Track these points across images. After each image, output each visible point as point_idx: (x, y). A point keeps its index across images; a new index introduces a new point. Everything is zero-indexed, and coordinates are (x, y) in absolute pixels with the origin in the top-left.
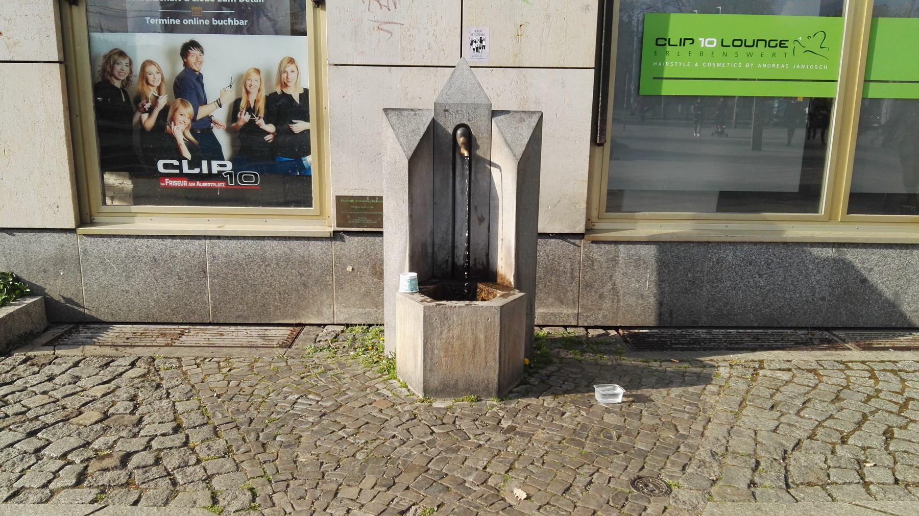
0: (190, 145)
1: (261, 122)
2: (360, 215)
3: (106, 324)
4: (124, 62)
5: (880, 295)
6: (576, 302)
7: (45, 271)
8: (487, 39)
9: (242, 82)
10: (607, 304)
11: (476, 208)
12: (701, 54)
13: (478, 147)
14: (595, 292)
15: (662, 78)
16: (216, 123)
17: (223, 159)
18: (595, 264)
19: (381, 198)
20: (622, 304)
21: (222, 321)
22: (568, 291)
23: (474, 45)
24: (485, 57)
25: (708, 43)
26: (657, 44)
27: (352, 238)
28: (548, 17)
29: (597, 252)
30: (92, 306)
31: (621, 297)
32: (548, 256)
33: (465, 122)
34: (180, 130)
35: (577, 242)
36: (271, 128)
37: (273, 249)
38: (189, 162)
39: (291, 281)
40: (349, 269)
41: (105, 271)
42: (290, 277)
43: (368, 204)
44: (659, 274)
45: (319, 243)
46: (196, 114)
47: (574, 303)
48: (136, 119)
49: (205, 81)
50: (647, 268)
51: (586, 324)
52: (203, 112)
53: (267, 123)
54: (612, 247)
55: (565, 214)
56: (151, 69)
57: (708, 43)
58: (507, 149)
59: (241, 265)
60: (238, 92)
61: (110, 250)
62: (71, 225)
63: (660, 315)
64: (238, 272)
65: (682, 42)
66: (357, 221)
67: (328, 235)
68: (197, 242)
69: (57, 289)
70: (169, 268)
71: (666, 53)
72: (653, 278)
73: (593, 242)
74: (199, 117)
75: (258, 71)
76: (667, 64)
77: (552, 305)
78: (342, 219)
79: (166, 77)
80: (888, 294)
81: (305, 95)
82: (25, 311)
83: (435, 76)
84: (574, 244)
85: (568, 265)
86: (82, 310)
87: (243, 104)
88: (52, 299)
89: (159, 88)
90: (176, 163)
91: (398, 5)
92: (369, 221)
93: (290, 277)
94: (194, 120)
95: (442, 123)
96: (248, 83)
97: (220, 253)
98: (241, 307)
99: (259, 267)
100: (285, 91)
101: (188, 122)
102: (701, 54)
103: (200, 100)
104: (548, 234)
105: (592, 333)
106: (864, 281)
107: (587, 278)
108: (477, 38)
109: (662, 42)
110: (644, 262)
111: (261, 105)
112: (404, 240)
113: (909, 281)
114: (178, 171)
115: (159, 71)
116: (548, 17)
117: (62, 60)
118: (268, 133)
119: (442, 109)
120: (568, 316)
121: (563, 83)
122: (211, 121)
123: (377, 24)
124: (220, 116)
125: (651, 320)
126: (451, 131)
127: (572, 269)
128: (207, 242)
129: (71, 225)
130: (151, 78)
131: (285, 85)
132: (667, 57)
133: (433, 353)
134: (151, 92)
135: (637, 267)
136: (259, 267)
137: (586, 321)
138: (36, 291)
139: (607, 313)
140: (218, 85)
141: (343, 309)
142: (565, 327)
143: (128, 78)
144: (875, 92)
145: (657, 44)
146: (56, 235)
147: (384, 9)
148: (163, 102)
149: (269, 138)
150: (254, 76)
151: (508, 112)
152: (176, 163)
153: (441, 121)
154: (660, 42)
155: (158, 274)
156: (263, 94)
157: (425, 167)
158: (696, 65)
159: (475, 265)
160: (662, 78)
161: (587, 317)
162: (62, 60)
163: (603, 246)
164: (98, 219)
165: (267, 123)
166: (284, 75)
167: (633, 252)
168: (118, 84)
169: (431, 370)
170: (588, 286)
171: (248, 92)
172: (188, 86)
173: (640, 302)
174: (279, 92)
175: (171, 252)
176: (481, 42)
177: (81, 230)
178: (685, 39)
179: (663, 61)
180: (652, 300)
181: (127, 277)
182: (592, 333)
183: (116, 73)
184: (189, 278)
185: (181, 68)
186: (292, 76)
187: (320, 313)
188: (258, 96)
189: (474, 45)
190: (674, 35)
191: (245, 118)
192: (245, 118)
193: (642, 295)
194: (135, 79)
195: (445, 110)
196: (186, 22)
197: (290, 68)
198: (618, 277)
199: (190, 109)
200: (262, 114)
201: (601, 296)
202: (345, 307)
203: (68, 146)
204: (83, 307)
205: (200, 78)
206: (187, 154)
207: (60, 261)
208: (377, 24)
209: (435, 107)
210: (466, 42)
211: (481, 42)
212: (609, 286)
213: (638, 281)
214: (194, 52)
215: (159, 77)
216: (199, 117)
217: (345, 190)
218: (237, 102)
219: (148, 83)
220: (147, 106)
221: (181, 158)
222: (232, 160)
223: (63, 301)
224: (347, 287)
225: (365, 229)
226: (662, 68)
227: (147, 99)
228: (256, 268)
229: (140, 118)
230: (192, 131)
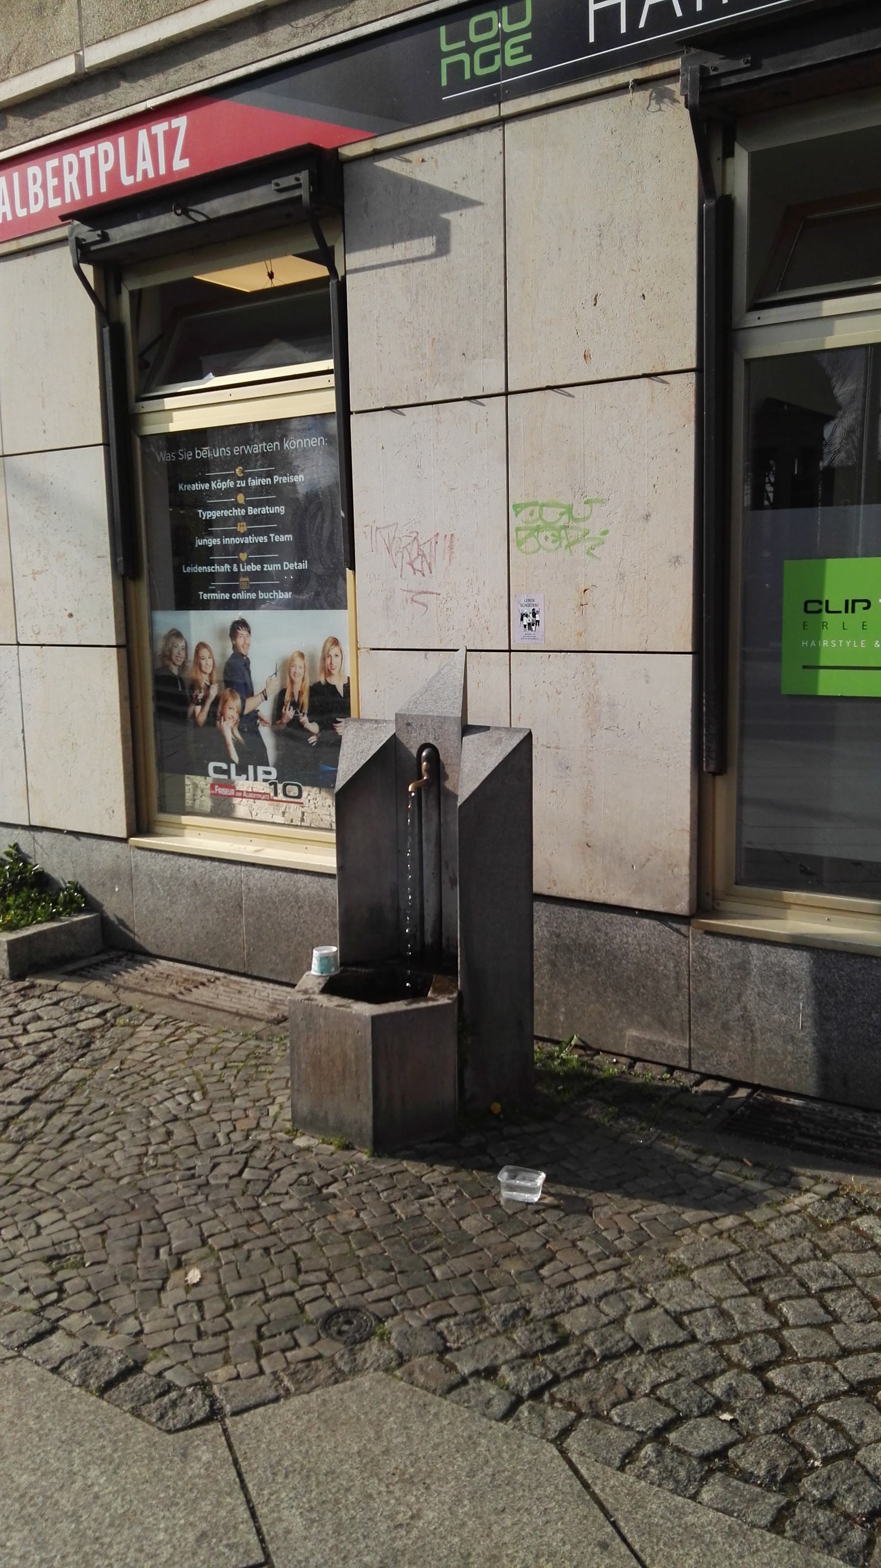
0: (237, 744)
1: (304, 719)
3: (149, 956)
4: (181, 644)
6: (687, 1028)
7: (104, 885)
8: (541, 612)
9: (286, 668)
10: (735, 1042)
11: (446, 863)
13: (446, 777)
14: (716, 1017)
16: (262, 720)
17: (267, 765)
18: (713, 969)
20: (759, 1046)
21: (255, 974)
22: (671, 1009)
23: (526, 621)
24: (543, 637)
28: (622, 576)
29: (714, 949)
30: (144, 936)
31: (758, 1034)
32: (639, 945)
33: (431, 741)
34: (229, 728)
35: (683, 928)
36: (314, 727)
37: (306, 887)
38: (237, 766)
39: (324, 932)
41: (152, 891)
42: (323, 927)
44: (819, 1004)
46: (243, 707)
47: (683, 1031)
48: (191, 710)
49: (252, 667)
50: (798, 990)
51: (703, 1070)
52: (251, 704)
53: (310, 721)
54: (738, 945)
55: (658, 881)
56: (204, 653)
59: (274, 903)
60: (283, 679)
61: (157, 868)
62: (123, 834)
63: (824, 1079)
64: (272, 912)
68: (233, 868)
69: (114, 906)
70: (208, 897)
71: (824, 625)
72: (809, 1011)
73: (707, 933)
74: (246, 712)
75: (302, 655)
76: (825, 643)
77: (648, 1027)
79: (217, 659)
81: (347, 687)
82: (68, 930)
83: (479, 663)
84: (678, 931)
85: (671, 965)
86: (132, 935)
87: (287, 697)
88: (107, 917)
89: (211, 675)
90: (224, 766)
93: (323, 927)
94: (241, 715)
95: (404, 741)
96: (293, 670)
97: (255, 885)
98: (274, 958)
99: (292, 908)
100: (329, 680)
101: (236, 716)
103: (247, 691)
104: (634, 910)
105: (708, 1086)
107: (700, 991)
108: (528, 610)
109: (815, 607)
110: (794, 980)
111: (305, 699)
114: (226, 777)
115: (211, 656)
116: (622, 576)
117: (123, 641)
118: (312, 734)
119: (404, 721)
120: (675, 1050)
121: (647, 676)
122: (257, 717)
123: (410, 595)
124: (266, 710)
125: (809, 1084)
126: (414, 752)
127: (677, 973)
128: (243, 868)
129: (123, 834)
130: (203, 662)
131: (328, 673)
132: (824, 632)
133: (300, 1066)
134: (204, 680)
135: (782, 986)
136: (292, 908)
137: (703, 1064)
138: (91, 905)
139: (736, 1057)
140: (263, 675)
142: (671, 1069)
143: (184, 663)
145: (806, 611)
146: (113, 843)
147: (419, 574)
148: (214, 692)
149: (313, 739)
150: (298, 662)
151: (486, 728)
152: (224, 766)
153: (403, 738)
154: (811, 607)
155: (198, 903)
156: (308, 684)
161: (705, 1058)
162: (124, 643)
163: (723, 941)
164: (159, 829)
165: (310, 721)
166: (328, 661)
167: (772, 959)
168: (175, 671)
170: (704, 1004)
171: (292, 682)
172: (237, 675)
173: (790, 1048)
174: (323, 681)
175: (210, 878)
176: (534, 616)
177: (133, 840)
178: (854, 601)
179: (818, 638)
180: (809, 1048)
181: (171, 902)
182: (708, 1086)
183: (174, 658)
184: (226, 912)
185: (230, 652)
186: (336, 661)
188: (302, 684)
189: (526, 621)
191: (289, 713)
192: (289, 713)
193: (792, 1038)
194: (190, 664)
196: (235, 596)
197: (334, 651)
198: (750, 998)
199: (238, 702)
200: (306, 711)
201: (726, 1027)
203: (124, 742)
204: (133, 932)
205: (247, 664)
206: (235, 756)
207: (115, 874)
208: (410, 595)
209: (396, 720)
210: (516, 617)
211: (534, 616)
212: (737, 1011)
213: (784, 1011)
214: (242, 632)
215: (210, 662)
216: (246, 712)
218: (283, 692)
219: (201, 671)
220: (201, 696)
221: (229, 761)
222: (276, 766)
223: (117, 923)
227: (200, 688)
228: (288, 909)
229: (194, 712)
230: (241, 730)
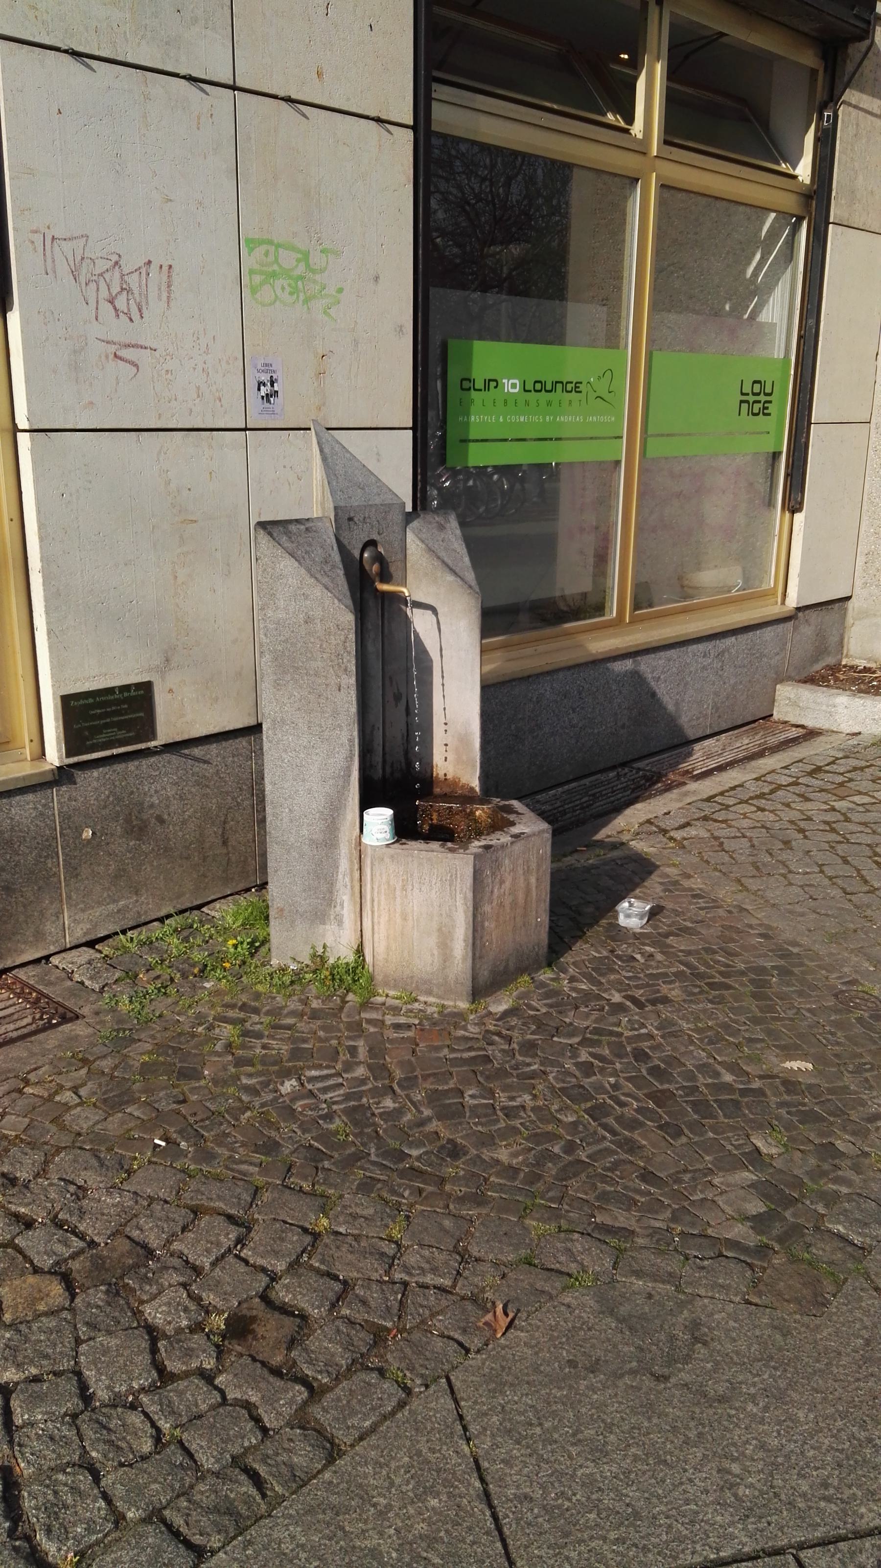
2: (106, 726)
5: (665, 709)
11: (391, 678)
12: (506, 402)
15: (470, 441)
19: (147, 687)
23: (264, 391)
25: (511, 386)
26: (462, 389)
27: (88, 773)
40: (88, 834)
43: (118, 702)
45: (30, 797)
57: (511, 386)
58: (450, 578)
65: (487, 383)
66: (102, 738)
67: (50, 778)
76: (473, 419)
78: (75, 737)
80: (671, 707)
91: (144, 310)
92: (122, 734)
102: (506, 402)
106: (654, 695)
108: (265, 378)
112: (343, 753)
113: (686, 684)
121: (378, 454)
123: (112, 348)
141: (80, 916)
144: (656, 448)
157: (834, 639)
158: (501, 420)
159: (392, 773)
160: (470, 441)
169: (480, 958)
178: (490, 380)
179: (468, 414)
187: (39, 936)
189: (264, 391)
190: (479, 375)
195: (350, 519)
202: (83, 911)
208: (112, 348)
217: (79, 684)
224: (85, 871)
225: (115, 751)
226: (467, 424)
